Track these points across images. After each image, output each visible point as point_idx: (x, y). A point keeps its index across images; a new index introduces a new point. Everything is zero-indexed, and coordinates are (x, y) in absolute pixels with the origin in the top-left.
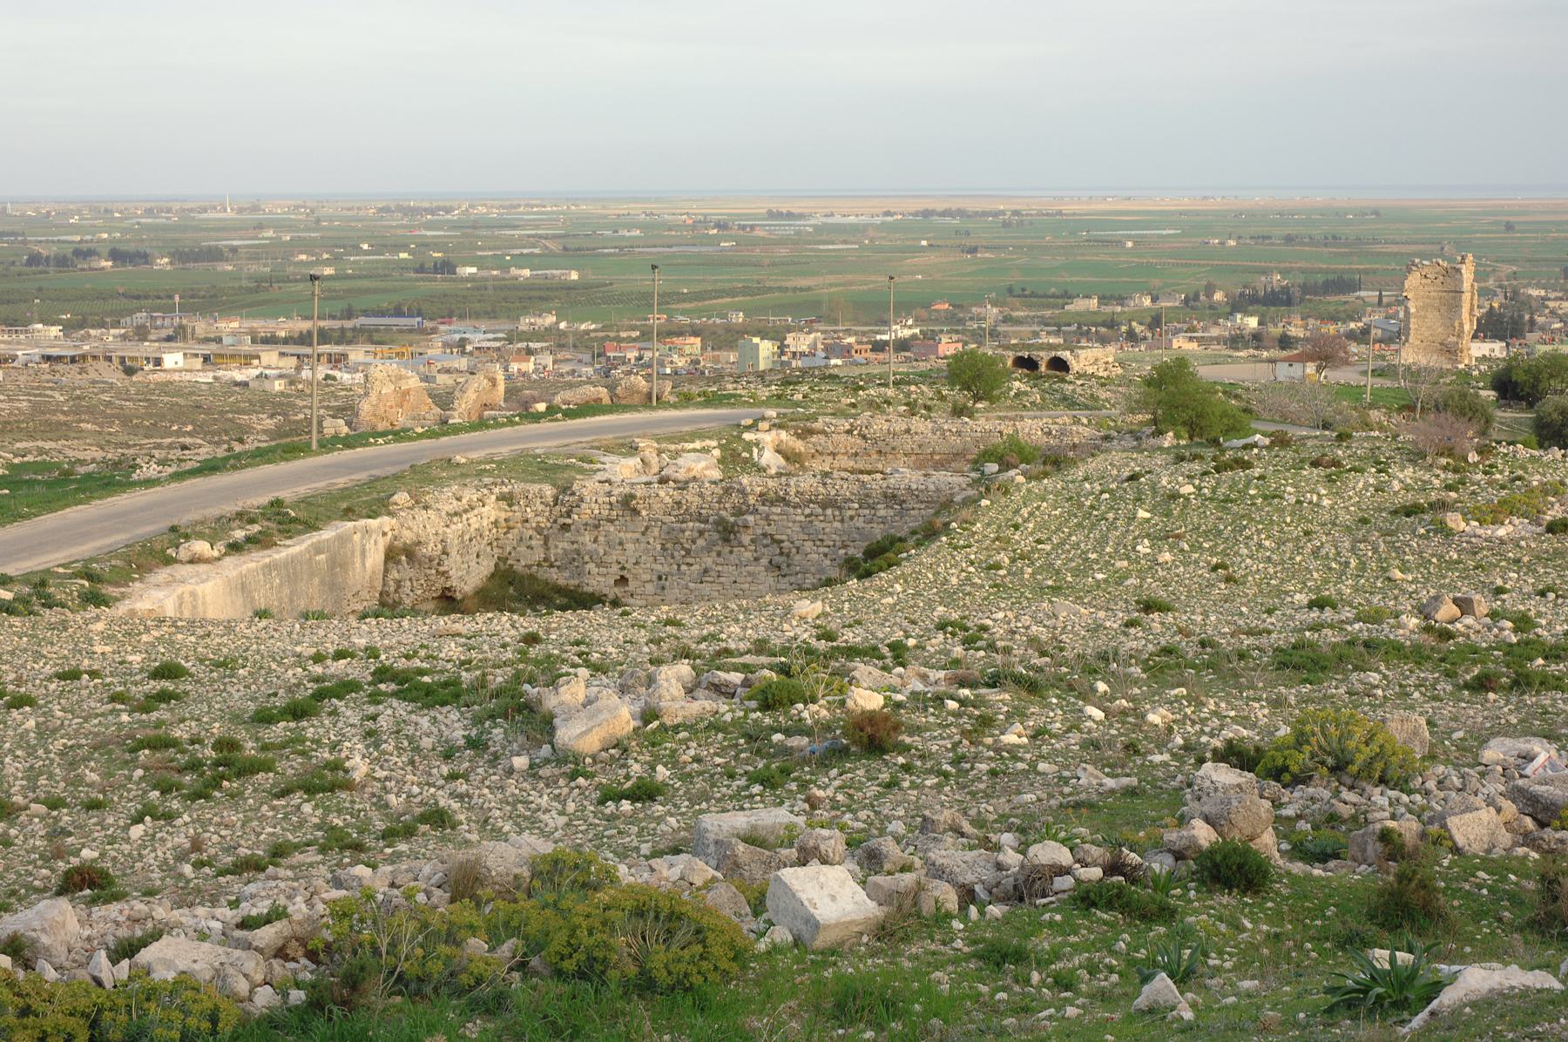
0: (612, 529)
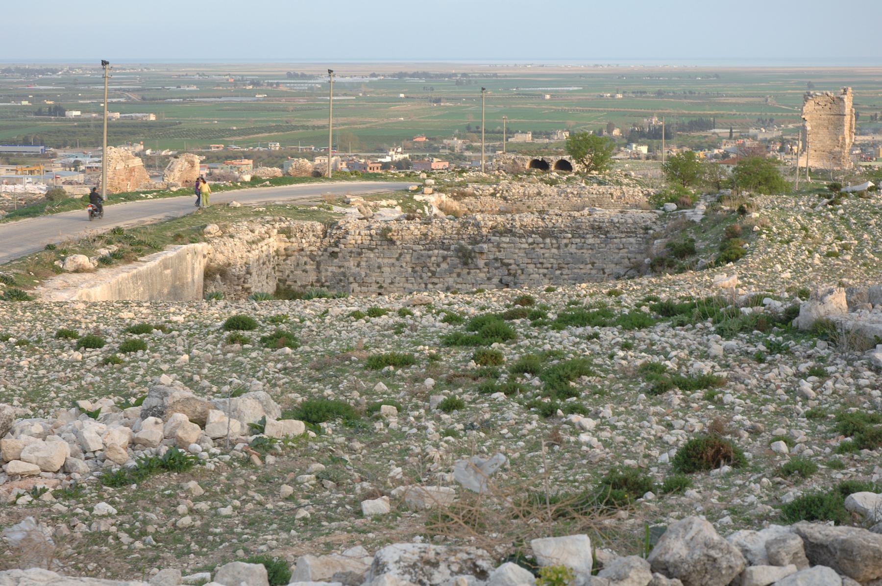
0: (372, 255)
